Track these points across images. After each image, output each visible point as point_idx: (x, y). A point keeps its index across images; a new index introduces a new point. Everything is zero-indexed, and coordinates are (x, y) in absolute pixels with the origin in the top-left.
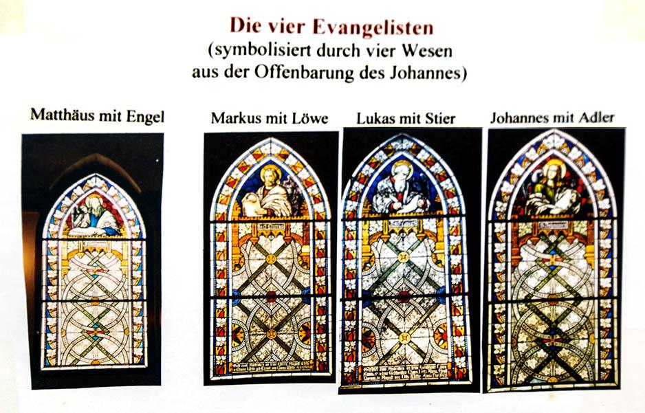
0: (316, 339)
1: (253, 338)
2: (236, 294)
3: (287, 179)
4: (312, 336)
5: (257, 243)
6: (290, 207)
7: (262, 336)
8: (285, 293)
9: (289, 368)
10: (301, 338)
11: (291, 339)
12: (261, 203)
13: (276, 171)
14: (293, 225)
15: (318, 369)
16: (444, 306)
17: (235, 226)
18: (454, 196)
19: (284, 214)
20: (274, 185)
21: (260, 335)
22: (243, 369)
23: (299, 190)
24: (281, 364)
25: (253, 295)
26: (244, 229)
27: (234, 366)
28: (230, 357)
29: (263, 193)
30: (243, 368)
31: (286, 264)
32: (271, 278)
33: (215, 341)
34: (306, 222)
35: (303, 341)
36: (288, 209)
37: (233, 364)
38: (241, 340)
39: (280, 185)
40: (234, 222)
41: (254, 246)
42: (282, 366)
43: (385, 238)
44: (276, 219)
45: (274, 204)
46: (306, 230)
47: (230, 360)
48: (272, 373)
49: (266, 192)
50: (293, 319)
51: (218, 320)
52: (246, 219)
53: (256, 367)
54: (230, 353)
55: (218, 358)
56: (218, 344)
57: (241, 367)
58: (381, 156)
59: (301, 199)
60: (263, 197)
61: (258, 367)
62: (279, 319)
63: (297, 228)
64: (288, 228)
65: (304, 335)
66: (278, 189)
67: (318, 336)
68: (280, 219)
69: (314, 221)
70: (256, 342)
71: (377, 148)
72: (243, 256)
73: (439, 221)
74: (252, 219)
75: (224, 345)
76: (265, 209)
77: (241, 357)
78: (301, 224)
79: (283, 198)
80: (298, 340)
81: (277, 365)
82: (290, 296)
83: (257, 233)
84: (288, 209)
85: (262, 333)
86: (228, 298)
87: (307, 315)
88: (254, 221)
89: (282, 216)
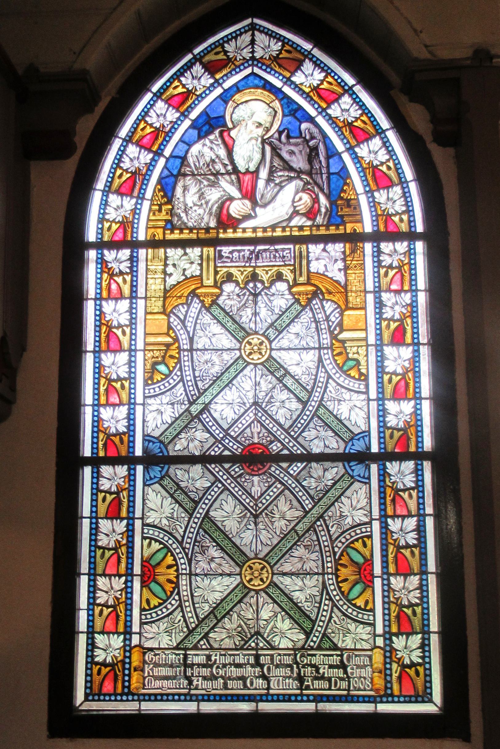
0: (388, 589)
5: (214, 302)
11: (313, 365)
14: (315, 249)
43: (206, 295)
62: (280, 525)
64: (300, 263)
72: (176, 340)
86: (130, 461)
87: (360, 517)
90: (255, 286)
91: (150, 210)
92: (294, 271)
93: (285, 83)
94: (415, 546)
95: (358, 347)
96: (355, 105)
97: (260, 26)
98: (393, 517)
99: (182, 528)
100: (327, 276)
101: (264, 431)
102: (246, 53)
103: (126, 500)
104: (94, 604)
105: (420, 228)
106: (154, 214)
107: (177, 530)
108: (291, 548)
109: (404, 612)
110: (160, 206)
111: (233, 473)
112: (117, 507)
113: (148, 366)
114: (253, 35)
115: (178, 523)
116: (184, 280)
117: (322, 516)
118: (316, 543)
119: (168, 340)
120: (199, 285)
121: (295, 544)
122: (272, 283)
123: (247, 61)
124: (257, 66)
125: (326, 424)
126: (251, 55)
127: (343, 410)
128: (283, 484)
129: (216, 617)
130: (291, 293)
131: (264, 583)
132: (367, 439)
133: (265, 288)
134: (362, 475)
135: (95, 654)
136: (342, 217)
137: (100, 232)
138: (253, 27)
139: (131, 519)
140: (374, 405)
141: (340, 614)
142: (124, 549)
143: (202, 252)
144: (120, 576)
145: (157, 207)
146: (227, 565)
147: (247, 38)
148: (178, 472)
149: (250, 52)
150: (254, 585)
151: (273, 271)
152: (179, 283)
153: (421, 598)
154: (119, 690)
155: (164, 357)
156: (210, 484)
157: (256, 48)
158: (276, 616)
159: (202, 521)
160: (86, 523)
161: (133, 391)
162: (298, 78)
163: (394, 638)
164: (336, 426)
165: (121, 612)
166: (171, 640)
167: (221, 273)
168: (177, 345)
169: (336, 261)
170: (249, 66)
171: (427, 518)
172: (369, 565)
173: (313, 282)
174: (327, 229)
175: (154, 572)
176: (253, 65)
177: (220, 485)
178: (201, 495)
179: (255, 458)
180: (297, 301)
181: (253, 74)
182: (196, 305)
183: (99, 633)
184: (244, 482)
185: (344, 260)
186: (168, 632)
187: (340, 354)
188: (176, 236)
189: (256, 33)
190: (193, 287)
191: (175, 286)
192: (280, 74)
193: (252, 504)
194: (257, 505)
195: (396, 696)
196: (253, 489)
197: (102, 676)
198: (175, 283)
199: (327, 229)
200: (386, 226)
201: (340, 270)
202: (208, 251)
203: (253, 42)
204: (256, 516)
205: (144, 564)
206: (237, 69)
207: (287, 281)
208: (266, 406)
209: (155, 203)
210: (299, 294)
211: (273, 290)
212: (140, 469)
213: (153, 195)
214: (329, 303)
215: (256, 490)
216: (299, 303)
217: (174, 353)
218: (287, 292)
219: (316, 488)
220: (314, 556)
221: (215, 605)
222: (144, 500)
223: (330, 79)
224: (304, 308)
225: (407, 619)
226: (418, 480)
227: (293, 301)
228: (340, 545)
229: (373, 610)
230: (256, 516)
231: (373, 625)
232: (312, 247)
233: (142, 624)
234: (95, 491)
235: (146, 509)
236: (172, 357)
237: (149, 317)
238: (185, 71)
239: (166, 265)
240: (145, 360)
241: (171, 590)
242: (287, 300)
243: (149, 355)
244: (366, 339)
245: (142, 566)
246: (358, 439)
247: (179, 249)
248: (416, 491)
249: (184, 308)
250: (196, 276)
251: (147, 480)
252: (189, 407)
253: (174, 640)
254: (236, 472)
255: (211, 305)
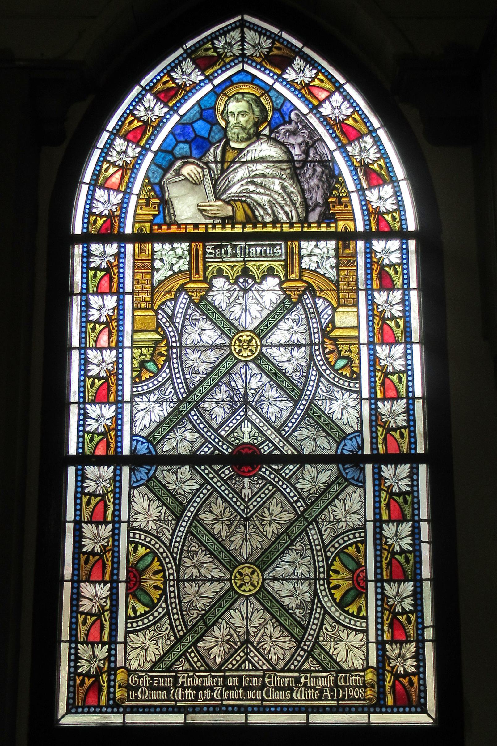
0: (382, 597)
1: (190, 589)
2: (351, 473)
3: (290, 122)
4: (371, 587)
5: (203, 298)
6: (297, 198)
7: (217, 587)
8: (288, 450)
9: (302, 697)
10: (338, 595)
11: (307, 597)
12: (214, 186)
13: (257, 100)
14: (307, 246)
15: (390, 701)
16: (137, 430)
17: (141, 251)
18: (385, 183)
19: (282, 217)
20: (254, 136)
21: (212, 580)
22: (158, 694)
23: (321, 148)
24: (278, 680)
25: (302, 465)
26: (170, 258)
27: (133, 680)
28: (120, 648)
29: (223, 161)
30: (158, 688)
31: (290, 361)
32: (246, 402)
33: (77, 596)
34: (346, 238)
35: (342, 605)
36: (294, 203)
37: (130, 672)
38: (155, 595)
39: (269, 138)
40: (139, 238)
41: (196, 305)
42: (277, 689)
43: (194, 290)
44: (259, 229)
45: (252, 188)
46: (345, 261)
47: (120, 661)
48: (244, 710)
49: (230, 156)
50: (313, 533)
51: (88, 530)
52: (174, 230)
53: (197, 689)
54: (121, 637)
55: (84, 651)
56: (86, 606)
57: (151, 687)
58: (149, 110)
59: (331, 176)
60: (223, 171)
61: (203, 688)
62: (271, 529)
63: (318, 255)
64: (292, 259)
65: (345, 585)
66: (265, 149)
67: (390, 590)
68: (269, 229)
69: (367, 236)
70: (200, 604)
71: (137, 90)
72: (165, 337)
73: (346, 247)
74: (190, 230)
75: (102, 610)
76: (228, 202)
77: (154, 652)
78: (332, 244)
79: (277, 173)
80: (327, 603)
81: (264, 685)
82: (301, 459)
83: (205, 269)
84: (294, 203)
85: (216, 573)
86: (116, 460)
87: (354, 520)
88: (196, 237)
89: (275, 221)
90: (246, 281)
91: (137, 204)
92: (285, 268)
93: (276, 80)
94: (411, 612)
95: (350, 344)
96: (346, 103)
97: (250, 23)
98: (383, 400)
99: (169, 531)
100: (318, 273)
101: (255, 430)
102: (236, 50)
103: (109, 563)
104: (88, 321)
105: (412, 226)
106: (141, 208)
107: (164, 534)
108: (283, 552)
109: (398, 619)
110: (148, 200)
111: (223, 475)
112: (103, 508)
113: (136, 364)
114: (242, 33)
115: (166, 526)
116: (171, 275)
117: (316, 642)
118: (308, 547)
119: (157, 336)
120: (188, 280)
121: (287, 548)
122: (263, 278)
123: (237, 57)
124: (247, 63)
125: (318, 424)
126: (240, 52)
127: (335, 409)
128: (274, 486)
129: (206, 624)
130: (282, 289)
131: (255, 587)
132: (359, 440)
133: (256, 283)
134: (356, 478)
135: (87, 423)
136: (334, 214)
137: (86, 224)
138: (242, 25)
139: (117, 521)
140: (366, 406)
141: (331, 621)
142: (107, 615)
143: (190, 246)
144: (105, 583)
145: (144, 201)
146: (217, 570)
147: (236, 34)
148: (167, 475)
149: (240, 50)
150: (244, 591)
151: (263, 266)
152: (167, 278)
153: (404, 311)
154: (103, 703)
155: (152, 355)
156: (198, 487)
157: (246, 46)
158: (267, 624)
159: (191, 524)
160: (70, 527)
161: (120, 388)
162: (290, 75)
163: (385, 526)
164: (327, 426)
165: (106, 621)
166: (157, 649)
167: (210, 268)
168: (165, 342)
169: (328, 258)
170: (239, 62)
171: (427, 644)
172: (362, 571)
173: (304, 278)
174: (319, 226)
175: (141, 579)
176: (243, 62)
177: (209, 487)
178: (189, 498)
179: (245, 459)
180: (288, 296)
181: (243, 70)
182: (183, 299)
183: (86, 523)
184: (235, 484)
185: (337, 257)
186: (159, 402)
187: (331, 352)
188: (164, 230)
189: (246, 30)
190: (181, 282)
191: (163, 281)
192: (271, 71)
193: (242, 507)
194: (247, 507)
195: (389, 706)
196: (243, 491)
197: (89, 566)
198: (163, 278)
199: (319, 226)
200: (378, 225)
201: (332, 267)
202: (197, 246)
203: (243, 40)
204: (247, 641)
205: (130, 569)
206: (226, 66)
207: (280, 278)
208: (258, 644)
209: (143, 197)
210: (290, 289)
211: (264, 286)
212: (126, 470)
213: (141, 190)
214: (321, 300)
215: (247, 492)
216: (290, 300)
217: (163, 350)
218: (277, 288)
219: (309, 490)
220: (301, 329)
221: (203, 612)
222: (130, 503)
223: (321, 76)
224: (295, 304)
225: (390, 332)
226: (407, 365)
227: (284, 296)
228: (332, 550)
229: (366, 618)
230: (247, 519)
231: (366, 632)
232: (304, 244)
233: (127, 633)
234: (81, 434)
235: (132, 513)
236: (161, 355)
237: (137, 313)
238: (176, 66)
239: (153, 260)
240: (133, 358)
241: (158, 597)
242: (278, 295)
243: (137, 352)
244: (358, 337)
245: (128, 572)
246: (351, 439)
247: (167, 244)
248: (407, 430)
249: (171, 303)
250: (185, 271)
251: (134, 482)
252: (179, 405)
253: (161, 649)
254: (226, 475)
255: (201, 301)
